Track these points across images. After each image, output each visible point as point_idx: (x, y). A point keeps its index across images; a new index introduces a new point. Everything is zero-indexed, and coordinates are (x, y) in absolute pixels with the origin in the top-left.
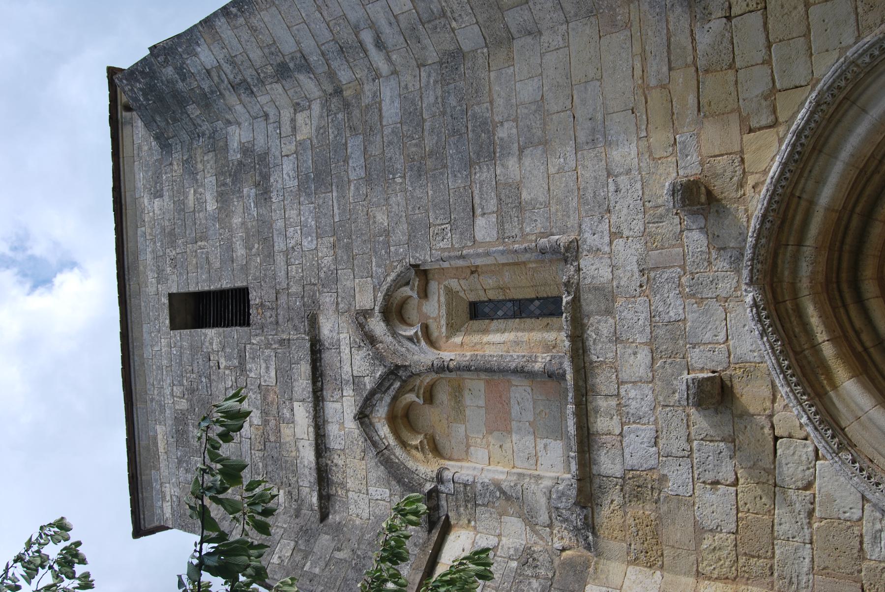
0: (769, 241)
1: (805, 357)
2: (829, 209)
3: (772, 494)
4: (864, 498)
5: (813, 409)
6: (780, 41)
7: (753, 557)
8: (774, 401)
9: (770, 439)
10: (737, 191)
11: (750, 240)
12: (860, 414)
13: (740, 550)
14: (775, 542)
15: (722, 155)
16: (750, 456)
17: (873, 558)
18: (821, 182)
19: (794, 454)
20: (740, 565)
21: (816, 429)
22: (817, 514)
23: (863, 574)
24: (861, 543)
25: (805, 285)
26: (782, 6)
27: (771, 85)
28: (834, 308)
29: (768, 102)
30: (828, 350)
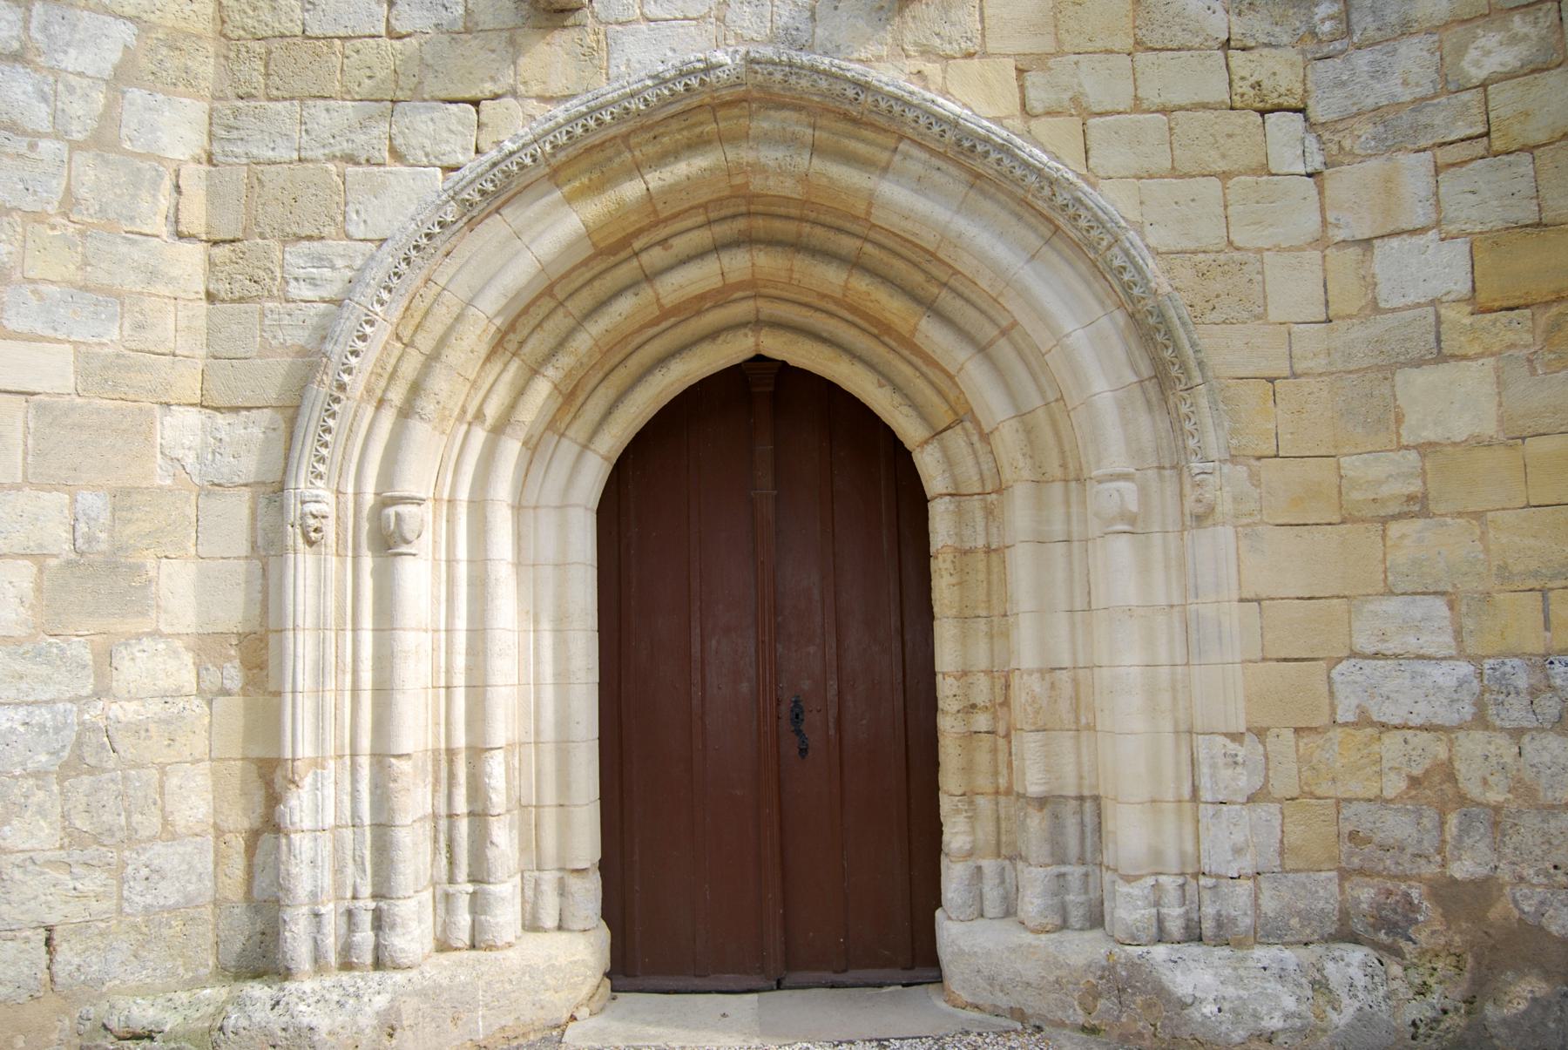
0: (822, 95)
1: (619, 154)
2: (871, 199)
3: (378, 96)
4: (384, 240)
5: (528, 161)
6: (1171, 129)
7: (266, 66)
8: (542, 98)
9: (473, 93)
10: (916, 44)
11: (824, 62)
12: (526, 239)
13: (276, 43)
14: (296, 102)
15: (982, 20)
16: (442, 57)
17: (287, 256)
18: (920, 185)
19: (451, 131)
20: (250, 44)
21: (495, 165)
22: (351, 169)
23: (259, 241)
24: (310, 238)
25: (743, 154)
26: (1230, 136)
27: (1096, 109)
28: (705, 206)
29: (1066, 103)
30: (632, 190)
